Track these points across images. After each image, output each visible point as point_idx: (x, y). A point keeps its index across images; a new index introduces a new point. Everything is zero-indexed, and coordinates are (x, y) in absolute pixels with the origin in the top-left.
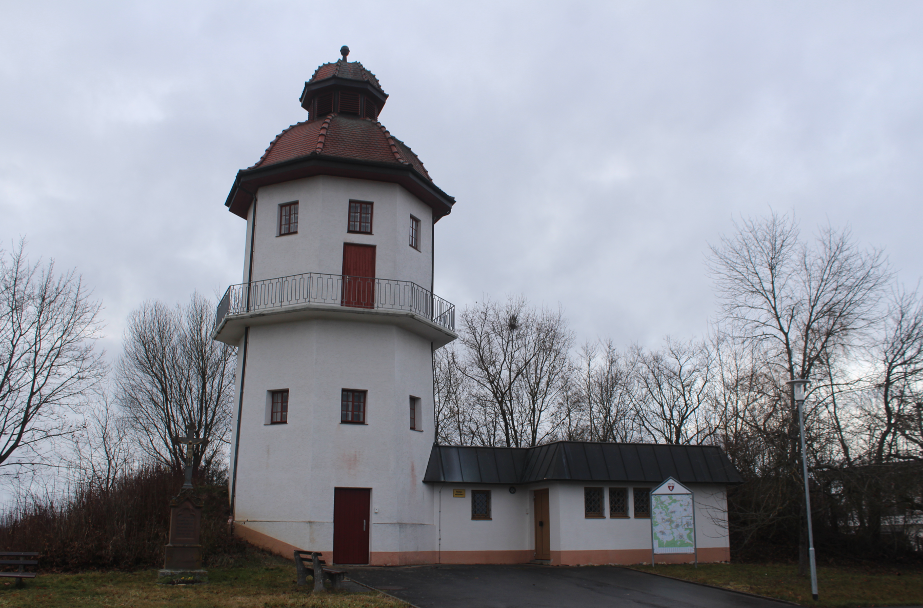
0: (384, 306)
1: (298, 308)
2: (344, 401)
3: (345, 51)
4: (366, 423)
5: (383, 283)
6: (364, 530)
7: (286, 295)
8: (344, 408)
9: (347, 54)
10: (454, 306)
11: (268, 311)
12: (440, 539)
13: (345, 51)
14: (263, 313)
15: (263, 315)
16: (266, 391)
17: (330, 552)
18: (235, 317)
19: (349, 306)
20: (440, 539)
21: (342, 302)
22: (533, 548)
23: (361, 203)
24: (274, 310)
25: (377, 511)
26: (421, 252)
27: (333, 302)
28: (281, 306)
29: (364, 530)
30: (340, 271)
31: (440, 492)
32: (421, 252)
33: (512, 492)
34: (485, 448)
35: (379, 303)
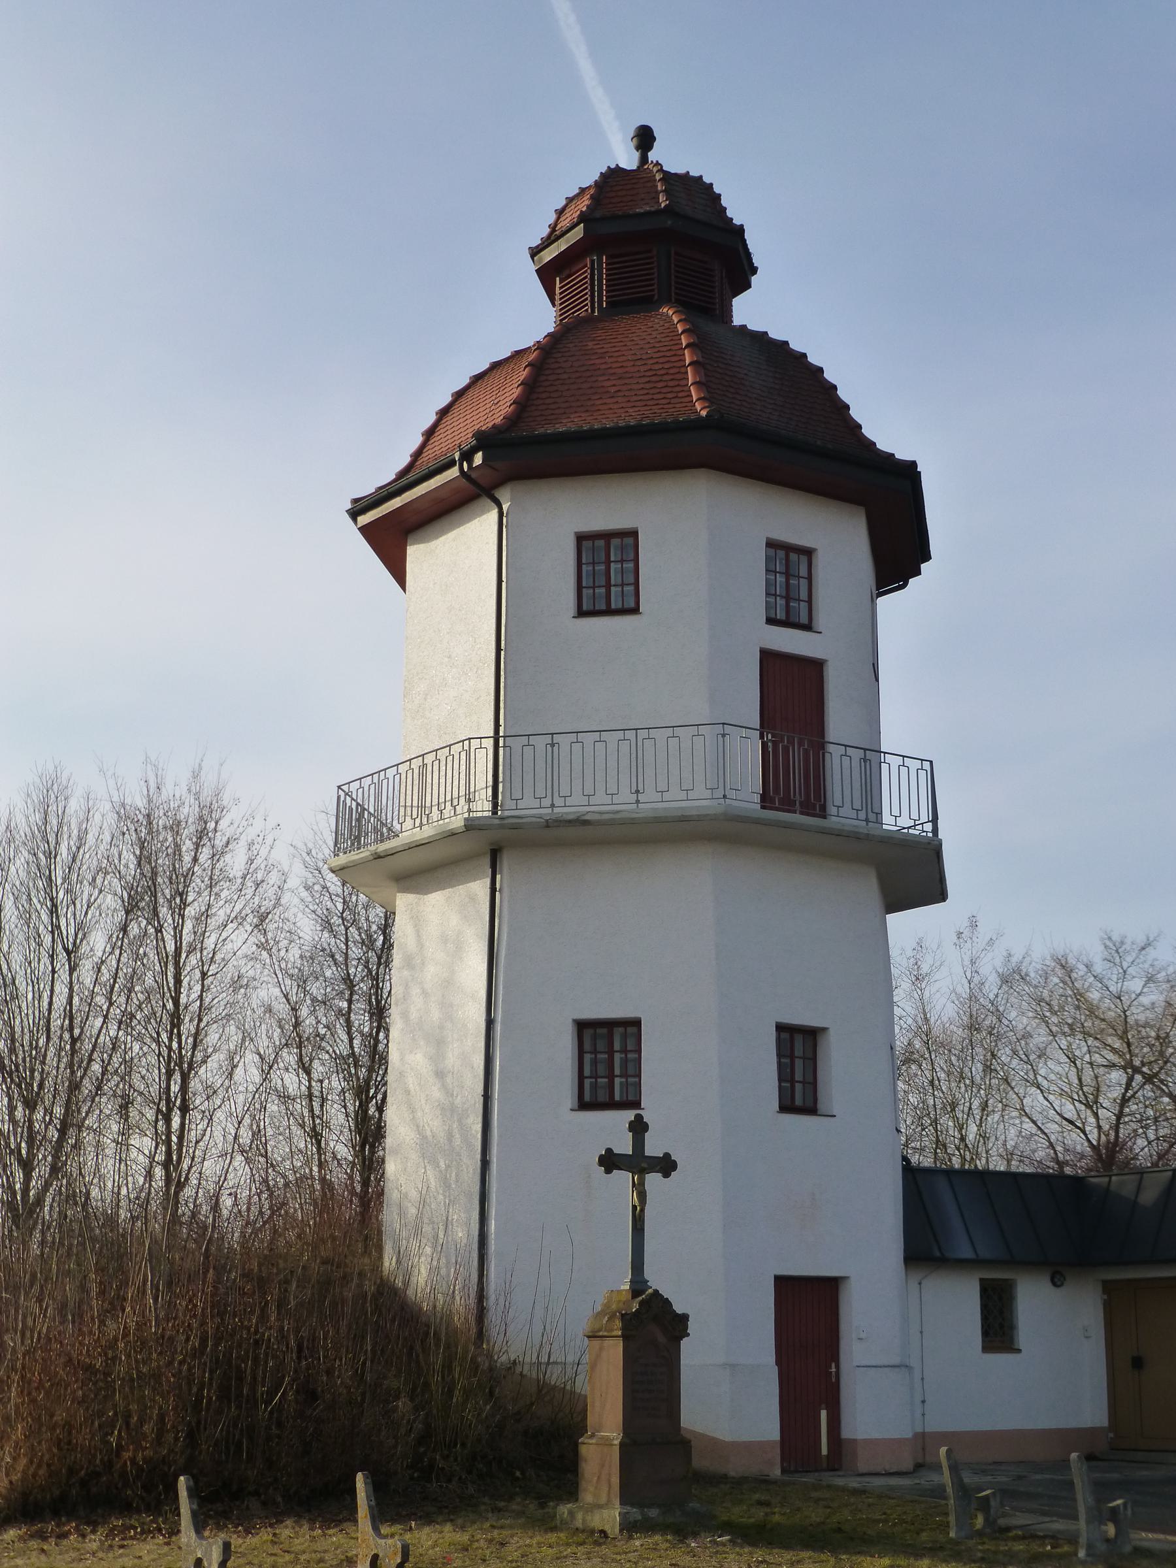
0: (569, 801)
1: (694, 813)
2: (784, 1056)
3: (645, 138)
4: (821, 1107)
5: (895, 761)
6: (834, 1380)
7: (540, 764)
8: (633, 1070)
9: (650, 147)
10: (339, 787)
11: (601, 813)
12: (923, 1402)
13: (645, 138)
14: (587, 817)
15: (586, 823)
16: (571, 1021)
17: (774, 1442)
18: (497, 822)
19: (808, 814)
20: (923, 1402)
21: (764, 797)
22: (1105, 1423)
23: (607, 536)
24: (618, 812)
25: (863, 1335)
26: (821, 633)
27: (683, 795)
28: (638, 802)
29: (834, 1380)
30: (755, 721)
31: (920, 1284)
32: (821, 633)
33: (1059, 1283)
34: (962, 1173)
35: (556, 795)
